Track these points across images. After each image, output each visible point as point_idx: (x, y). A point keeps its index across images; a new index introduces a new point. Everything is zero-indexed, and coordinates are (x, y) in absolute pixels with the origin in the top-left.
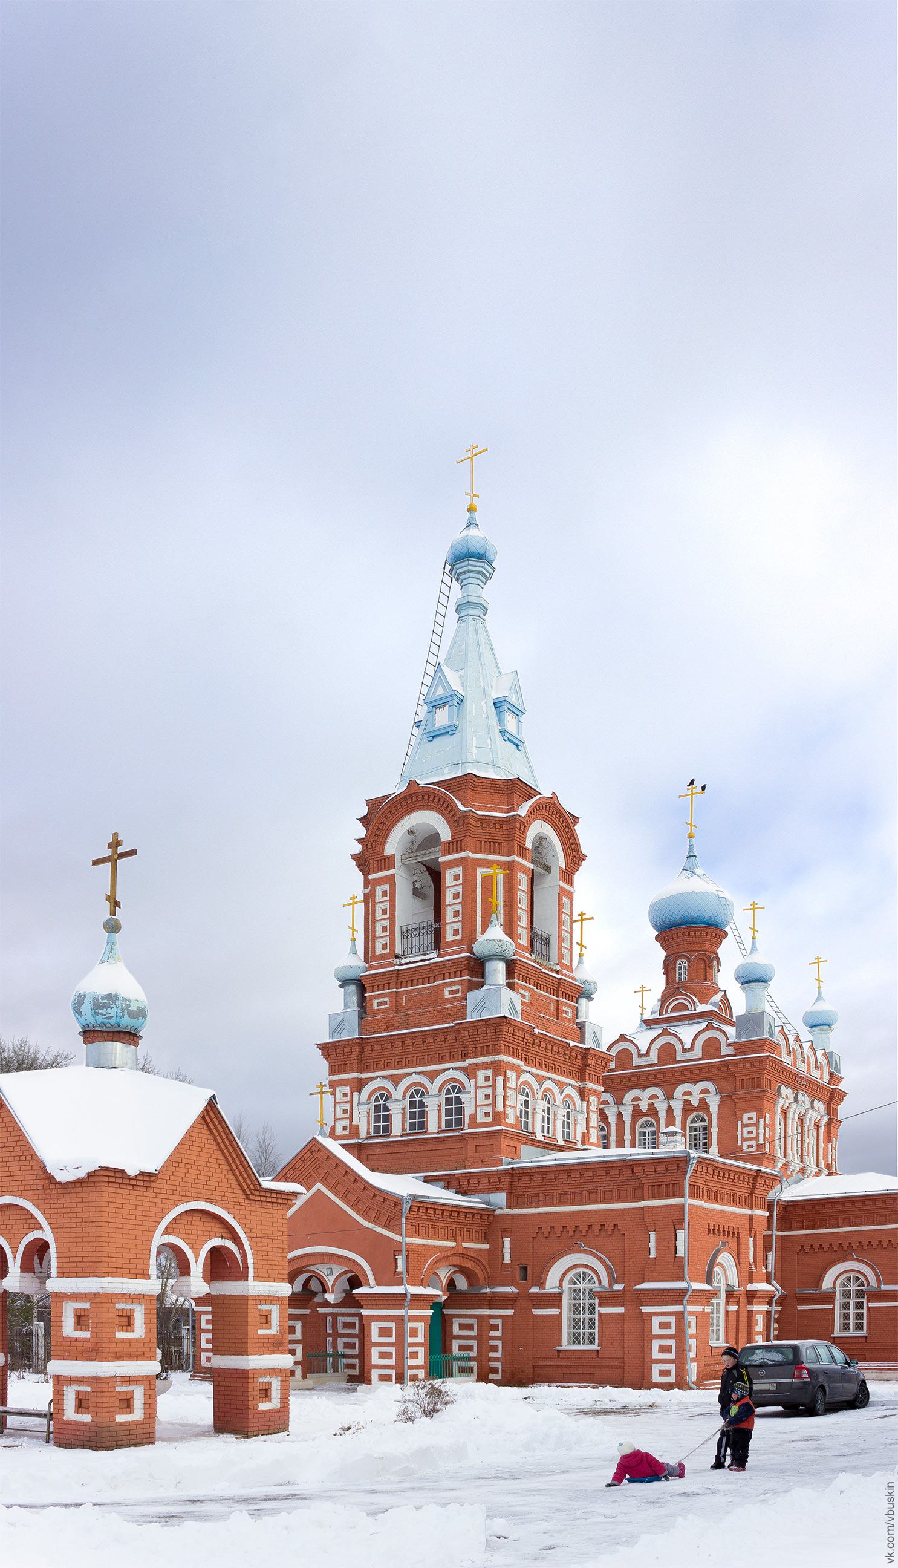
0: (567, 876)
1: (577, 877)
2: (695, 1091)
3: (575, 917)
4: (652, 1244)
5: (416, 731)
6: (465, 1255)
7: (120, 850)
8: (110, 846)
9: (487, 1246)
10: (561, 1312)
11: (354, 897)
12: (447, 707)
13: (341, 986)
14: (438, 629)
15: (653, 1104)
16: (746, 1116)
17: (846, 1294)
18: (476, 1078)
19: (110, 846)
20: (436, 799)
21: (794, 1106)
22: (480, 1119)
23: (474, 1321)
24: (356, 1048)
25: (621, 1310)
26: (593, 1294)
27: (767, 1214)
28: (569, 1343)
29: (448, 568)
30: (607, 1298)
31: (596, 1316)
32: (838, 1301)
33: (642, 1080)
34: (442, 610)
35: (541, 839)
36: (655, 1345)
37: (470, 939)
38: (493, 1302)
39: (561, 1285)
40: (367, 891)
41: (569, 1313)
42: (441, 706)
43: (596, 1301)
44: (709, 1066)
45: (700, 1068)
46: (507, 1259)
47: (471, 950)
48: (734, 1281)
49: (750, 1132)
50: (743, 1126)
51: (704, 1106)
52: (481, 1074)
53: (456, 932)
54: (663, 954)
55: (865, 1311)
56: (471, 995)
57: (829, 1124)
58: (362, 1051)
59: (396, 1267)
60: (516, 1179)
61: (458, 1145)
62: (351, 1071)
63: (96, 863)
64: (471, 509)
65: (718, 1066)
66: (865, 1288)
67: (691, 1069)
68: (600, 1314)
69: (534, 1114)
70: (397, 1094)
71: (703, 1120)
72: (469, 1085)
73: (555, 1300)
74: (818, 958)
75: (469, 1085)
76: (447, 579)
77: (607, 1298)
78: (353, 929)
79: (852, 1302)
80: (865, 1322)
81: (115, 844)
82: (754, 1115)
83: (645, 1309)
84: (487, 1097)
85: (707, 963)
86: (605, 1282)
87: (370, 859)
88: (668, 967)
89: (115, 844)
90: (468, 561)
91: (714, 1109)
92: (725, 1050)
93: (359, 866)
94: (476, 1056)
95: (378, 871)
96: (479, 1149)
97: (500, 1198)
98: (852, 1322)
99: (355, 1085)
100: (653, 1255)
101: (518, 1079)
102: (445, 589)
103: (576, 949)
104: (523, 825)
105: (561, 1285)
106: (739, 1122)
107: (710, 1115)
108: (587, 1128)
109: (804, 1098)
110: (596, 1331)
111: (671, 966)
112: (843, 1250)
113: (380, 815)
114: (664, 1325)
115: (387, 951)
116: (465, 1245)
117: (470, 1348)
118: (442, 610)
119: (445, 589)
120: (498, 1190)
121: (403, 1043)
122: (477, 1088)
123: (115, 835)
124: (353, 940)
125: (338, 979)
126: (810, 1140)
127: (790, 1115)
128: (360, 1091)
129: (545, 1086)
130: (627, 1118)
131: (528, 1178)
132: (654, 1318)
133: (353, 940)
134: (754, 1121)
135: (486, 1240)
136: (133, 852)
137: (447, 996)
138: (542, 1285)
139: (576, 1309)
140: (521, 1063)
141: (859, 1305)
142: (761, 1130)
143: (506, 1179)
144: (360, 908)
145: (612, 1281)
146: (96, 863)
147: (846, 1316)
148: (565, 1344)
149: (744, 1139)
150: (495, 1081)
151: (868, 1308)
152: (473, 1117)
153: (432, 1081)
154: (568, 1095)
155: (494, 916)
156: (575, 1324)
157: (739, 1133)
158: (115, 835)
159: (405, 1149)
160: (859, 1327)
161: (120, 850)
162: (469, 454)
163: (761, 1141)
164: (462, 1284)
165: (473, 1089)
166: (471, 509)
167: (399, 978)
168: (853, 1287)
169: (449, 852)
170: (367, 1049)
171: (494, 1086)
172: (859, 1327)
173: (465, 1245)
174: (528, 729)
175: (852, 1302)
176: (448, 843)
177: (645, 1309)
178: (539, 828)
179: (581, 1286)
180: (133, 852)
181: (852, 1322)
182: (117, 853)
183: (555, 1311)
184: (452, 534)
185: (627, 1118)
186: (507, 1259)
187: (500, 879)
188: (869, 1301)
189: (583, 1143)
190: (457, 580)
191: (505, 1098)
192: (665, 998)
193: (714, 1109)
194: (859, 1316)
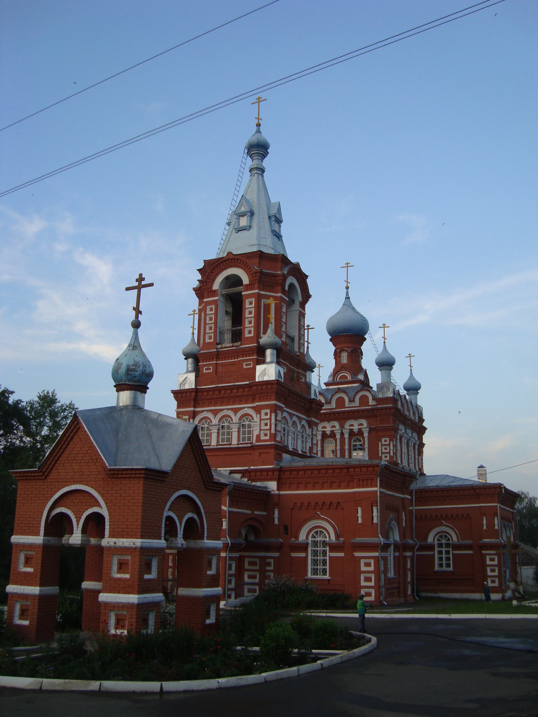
0: (303, 305)
1: (307, 306)
2: (355, 425)
3: (306, 328)
4: (360, 514)
5: (227, 227)
6: (255, 519)
7: (143, 283)
8: (137, 280)
9: (265, 513)
10: (307, 556)
11: (194, 311)
12: (246, 217)
13: (185, 359)
14: (240, 179)
15: (333, 431)
16: (383, 440)
17: (440, 545)
18: (260, 414)
19: (137, 280)
20: (242, 262)
21: (405, 435)
22: (263, 438)
23: (258, 560)
24: (193, 394)
25: (471, 552)
26: (324, 544)
27: (410, 497)
28: (311, 575)
29: (246, 151)
30: (334, 547)
31: (328, 558)
32: (437, 549)
33: (330, 417)
34: (242, 170)
35: (292, 285)
36: (488, 569)
37: (258, 336)
38: (267, 548)
39: (307, 538)
40: (201, 307)
41: (311, 556)
42: (243, 216)
43: (328, 549)
44: (363, 411)
45: (358, 411)
46: (276, 522)
47: (258, 342)
48: (397, 538)
49: (386, 449)
50: (382, 445)
51: (360, 432)
52: (263, 412)
53: (250, 332)
54: (334, 348)
55: (451, 556)
56: (258, 367)
57: (419, 446)
58: (196, 396)
59: (222, 526)
60: (282, 473)
61: (249, 452)
62: (189, 407)
63: (128, 289)
64: (258, 125)
65: (368, 410)
66: (451, 542)
67: (353, 412)
68: (330, 557)
69: (288, 435)
70: (215, 421)
71: (360, 441)
72: (256, 418)
73: (304, 547)
74: (410, 354)
75: (256, 418)
76: (245, 156)
77: (334, 547)
78: (193, 328)
79: (444, 550)
80: (451, 562)
81: (141, 279)
82: (388, 439)
83: (484, 552)
84: (266, 425)
85: (356, 355)
86: (333, 537)
87: (202, 291)
88: (337, 355)
89: (141, 279)
90: (259, 149)
91: (366, 435)
92: (371, 402)
93: (197, 294)
94: (260, 401)
95: (208, 297)
96: (261, 455)
97: (272, 485)
98: (444, 562)
99: (192, 415)
100: (360, 521)
101: (282, 415)
102: (244, 161)
103: (306, 344)
104: (285, 277)
105: (307, 538)
106: (380, 443)
107: (364, 438)
108: (312, 444)
109: (409, 431)
110: (328, 567)
111: (338, 355)
112: (436, 519)
113: (210, 269)
114: (368, 565)
115: (212, 340)
116: (256, 512)
117: (254, 577)
118: (242, 170)
119: (244, 161)
120: (272, 479)
121: (220, 392)
122: (261, 420)
123: (141, 275)
124: (193, 334)
125: (184, 355)
126: (411, 453)
127: (403, 439)
128: (194, 418)
129: (293, 419)
130: (346, 436)
131: (289, 473)
132: (362, 560)
133: (193, 334)
134: (388, 443)
135: (265, 510)
136: (151, 285)
137: (245, 367)
138: (297, 537)
139: (315, 553)
140: (283, 406)
141: (448, 552)
142: (392, 448)
143: (277, 473)
144: (197, 316)
145: (337, 537)
146: (128, 289)
147: (441, 559)
148: (310, 575)
149: (382, 453)
150: (271, 415)
151: (453, 554)
152: (258, 436)
153: (236, 414)
154: (303, 425)
155: (270, 325)
156: (315, 562)
157: (380, 449)
158: (141, 275)
159: (219, 453)
160: (448, 565)
161: (143, 283)
162: (257, 100)
163: (392, 454)
164: (252, 538)
165: (258, 420)
166: (258, 125)
167: (218, 355)
168: (444, 541)
169: (247, 290)
170: (200, 394)
171: (270, 419)
172: (448, 565)
173: (256, 512)
174: (285, 230)
175: (444, 550)
176: (247, 285)
177: (484, 552)
178: (291, 280)
179: (319, 539)
180: (151, 285)
181: (444, 562)
182: (141, 284)
183: (303, 555)
184: (248, 135)
185: (346, 436)
186: (276, 522)
187: (273, 306)
188: (453, 550)
189: (310, 453)
190: (250, 157)
191: (276, 425)
192: (335, 373)
193: (366, 435)
194: (448, 559)
